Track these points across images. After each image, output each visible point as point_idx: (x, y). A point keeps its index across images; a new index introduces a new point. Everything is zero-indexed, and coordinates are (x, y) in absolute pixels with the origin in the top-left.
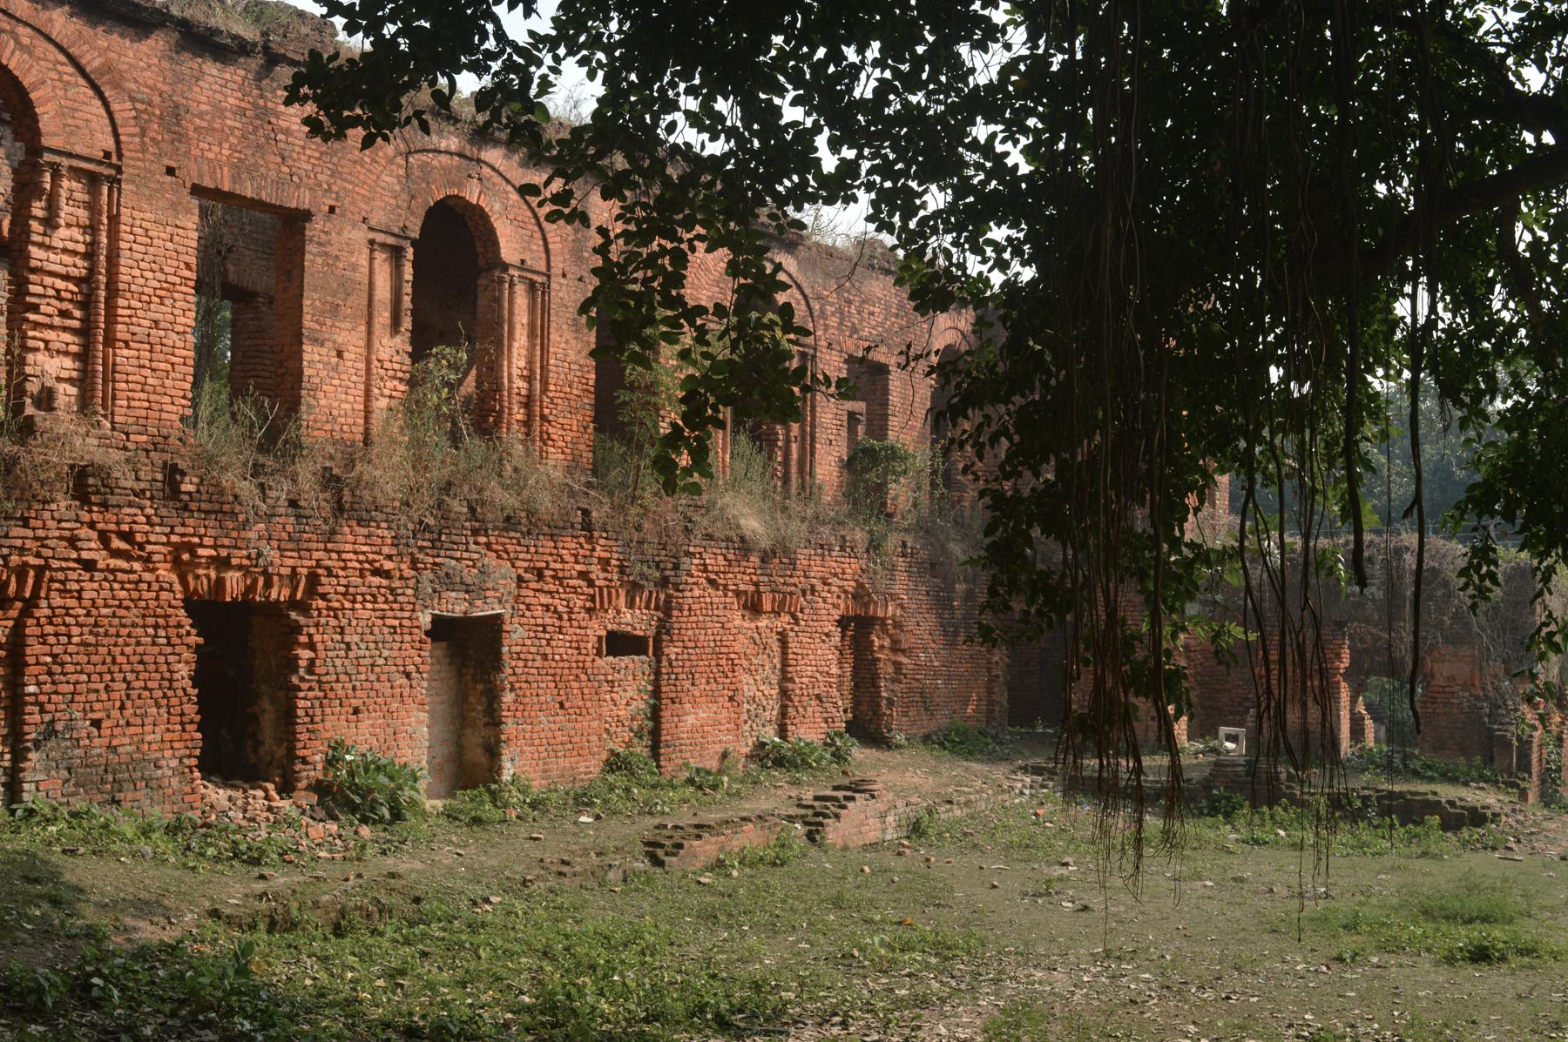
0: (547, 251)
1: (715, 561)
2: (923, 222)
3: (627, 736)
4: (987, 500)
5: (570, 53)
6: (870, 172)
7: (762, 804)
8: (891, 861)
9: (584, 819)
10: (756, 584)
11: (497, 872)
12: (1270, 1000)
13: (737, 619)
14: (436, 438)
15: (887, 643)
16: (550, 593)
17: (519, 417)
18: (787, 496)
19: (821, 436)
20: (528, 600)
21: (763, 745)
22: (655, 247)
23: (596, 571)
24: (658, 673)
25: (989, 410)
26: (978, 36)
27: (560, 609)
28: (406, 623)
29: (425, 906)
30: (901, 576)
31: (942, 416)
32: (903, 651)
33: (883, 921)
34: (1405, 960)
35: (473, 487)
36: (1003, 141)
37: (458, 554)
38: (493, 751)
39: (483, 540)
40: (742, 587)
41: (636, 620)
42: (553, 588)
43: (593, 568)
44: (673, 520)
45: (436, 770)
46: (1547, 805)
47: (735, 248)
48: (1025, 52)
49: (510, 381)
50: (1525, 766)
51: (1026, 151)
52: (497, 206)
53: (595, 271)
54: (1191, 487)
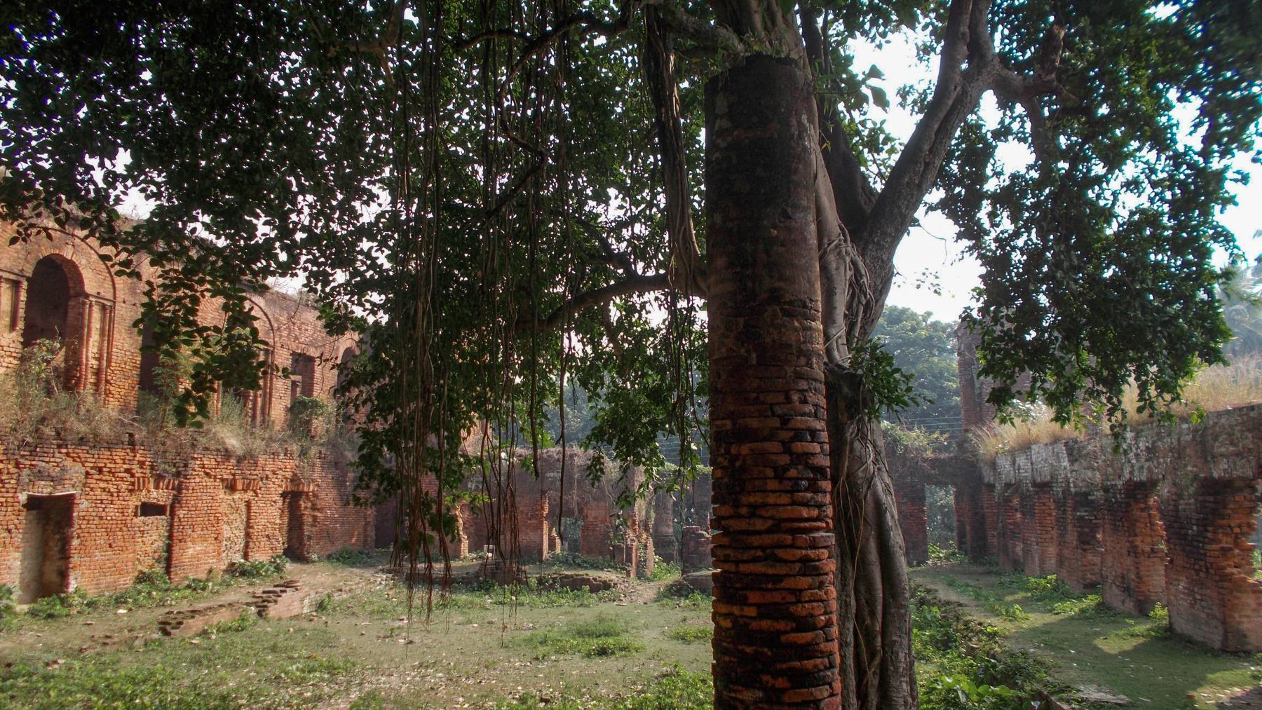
0: (114, 288)
1: (209, 462)
2: (333, 289)
3: (151, 562)
4: (360, 433)
5: (135, 185)
6: (306, 262)
7: (231, 597)
8: (306, 625)
9: (121, 611)
10: (234, 475)
11: (63, 646)
12: (501, 681)
13: (222, 494)
14: (35, 391)
15: (309, 505)
16: (106, 481)
17: (92, 381)
18: (254, 426)
19: (276, 394)
20: (778, 410)
21: (233, 564)
22: (181, 293)
23: (136, 469)
24: (171, 526)
25: (362, 388)
26: (365, 198)
27: (112, 490)
28: (9, 500)
29: (13, 669)
30: (318, 469)
31: (341, 390)
32: (318, 510)
33: (299, 657)
34: (568, 657)
35: (59, 420)
36: (376, 251)
37: (47, 459)
38: (63, 575)
39: (64, 451)
40: (225, 477)
41: (159, 495)
42: (108, 478)
43: (134, 467)
44: (185, 440)
45: (25, 587)
46: (639, 578)
47: (227, 297)
48: (389, 208)
49: (87, 360)
50: (629, 560)
51: (388, 257)
52: (84, 262)
53: (143, 305)
54: (464, 427)
